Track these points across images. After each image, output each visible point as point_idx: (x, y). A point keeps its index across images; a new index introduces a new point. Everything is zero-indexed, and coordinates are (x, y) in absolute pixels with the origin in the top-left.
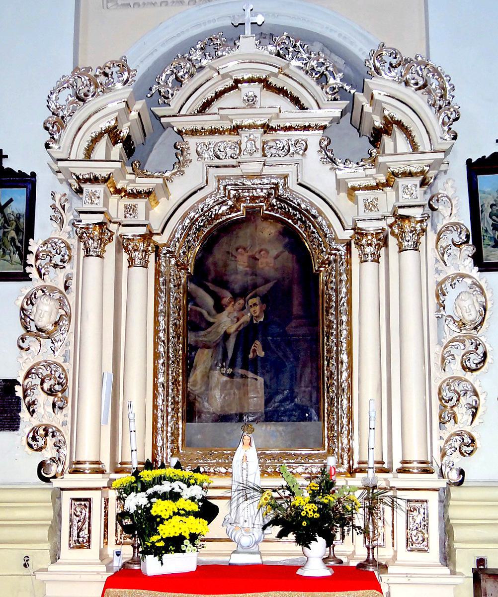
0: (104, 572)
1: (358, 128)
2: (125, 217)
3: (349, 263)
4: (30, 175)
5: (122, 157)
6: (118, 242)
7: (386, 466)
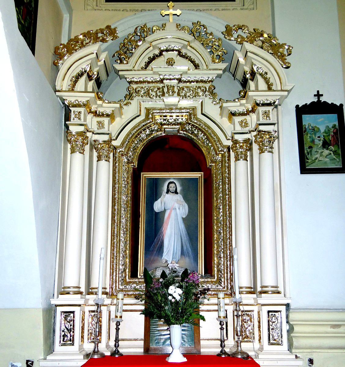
0: (82, 359)
1: (233, 74)
3: (229, 160)
6: (91, 144)
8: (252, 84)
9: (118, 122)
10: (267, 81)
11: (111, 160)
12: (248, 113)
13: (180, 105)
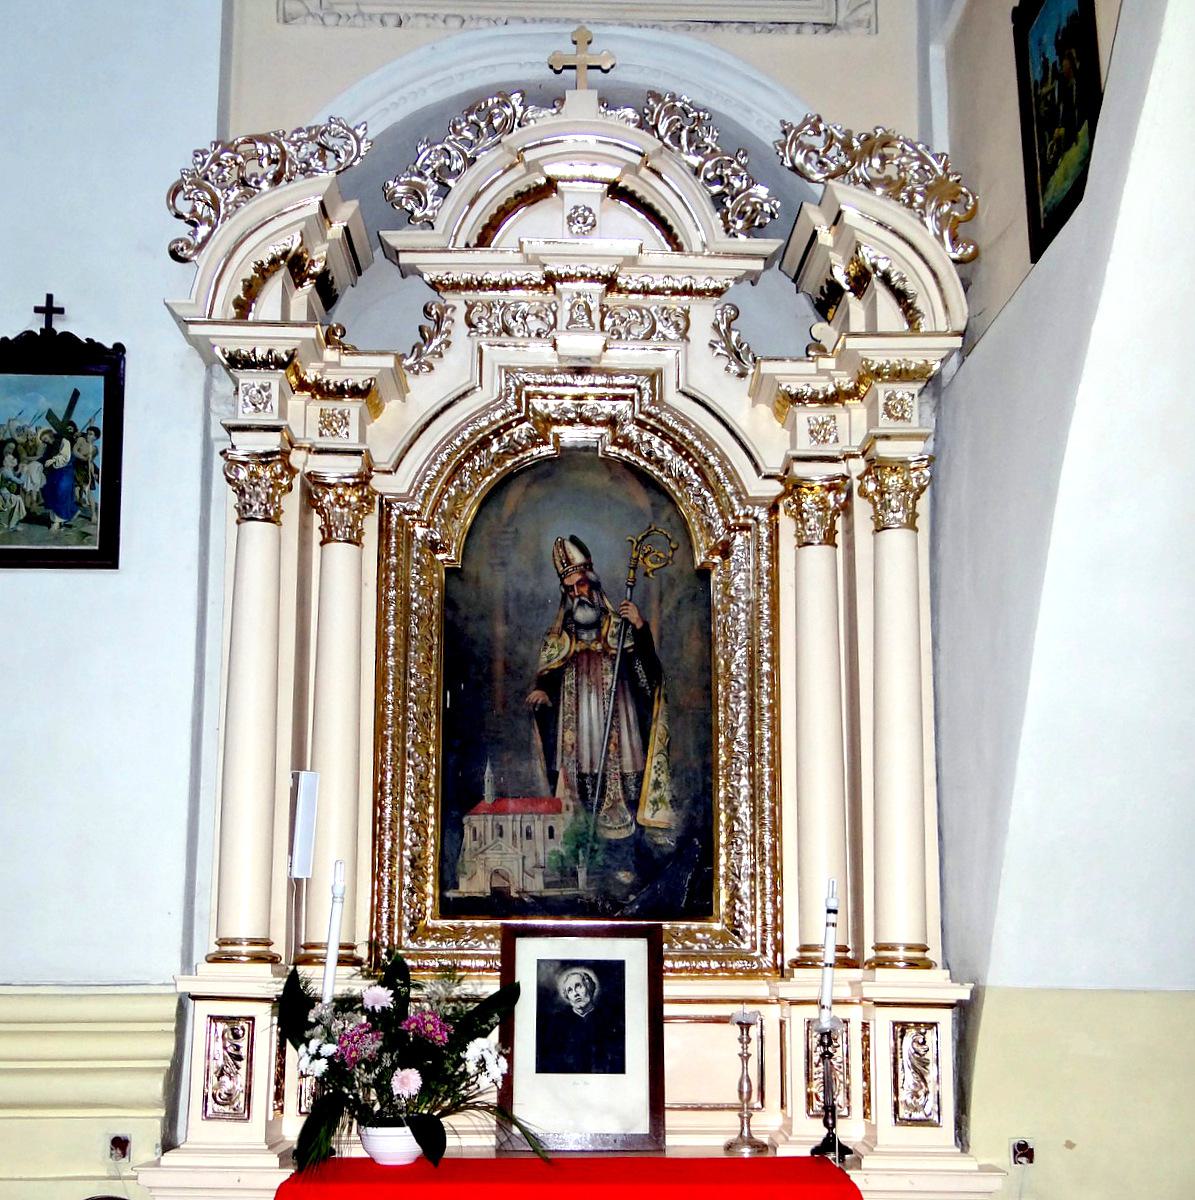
2: (321, 435)
4: (39, 333)
5: (313, 313)
7: (850, 955)
8: (854, 306)
9: (396, 418)
10: (900, 296)
11: (923, 522)
12: (836, 397)
13: (610, 358)
